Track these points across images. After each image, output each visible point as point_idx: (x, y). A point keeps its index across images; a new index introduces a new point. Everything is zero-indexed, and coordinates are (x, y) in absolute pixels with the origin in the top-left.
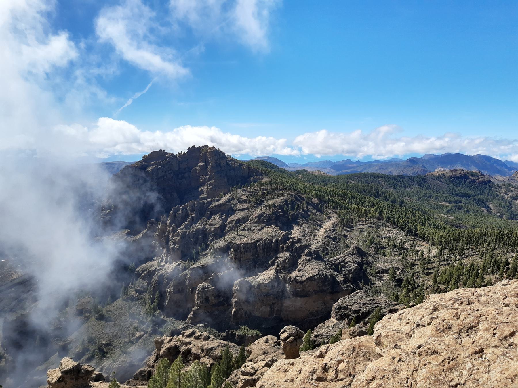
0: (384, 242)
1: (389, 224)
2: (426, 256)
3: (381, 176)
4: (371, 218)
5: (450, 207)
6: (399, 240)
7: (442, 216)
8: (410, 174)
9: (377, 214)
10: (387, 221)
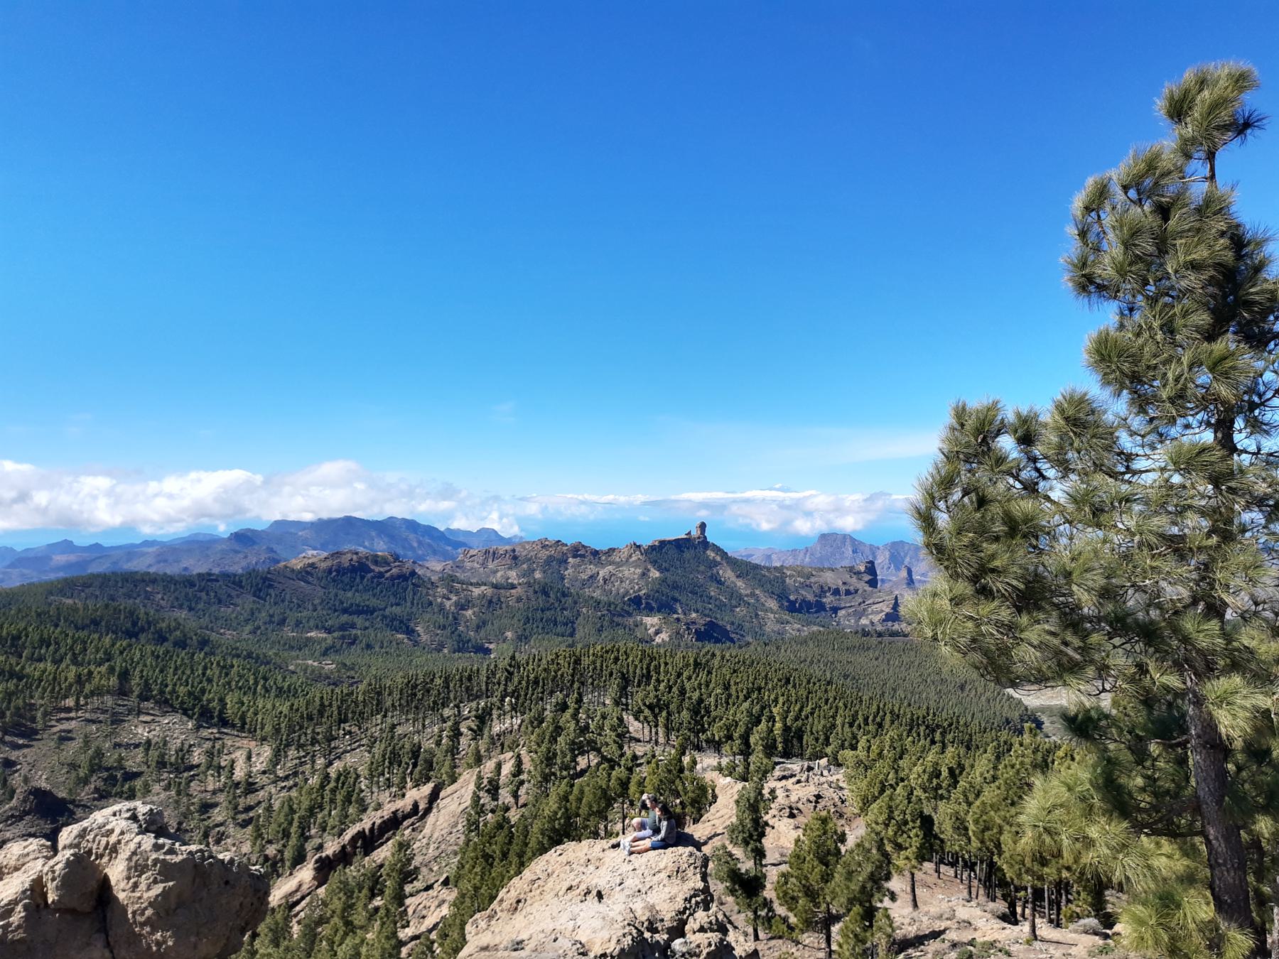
0: (134, 761)
1: (149, 704)
2: (239, 774)
3: (153, 580)
4: (92, 693)
5: (329, 641)
6: (174, 745)
7: (307, 666)
8: (237, 569)
9: (114, 681)
10: (144, 697)
